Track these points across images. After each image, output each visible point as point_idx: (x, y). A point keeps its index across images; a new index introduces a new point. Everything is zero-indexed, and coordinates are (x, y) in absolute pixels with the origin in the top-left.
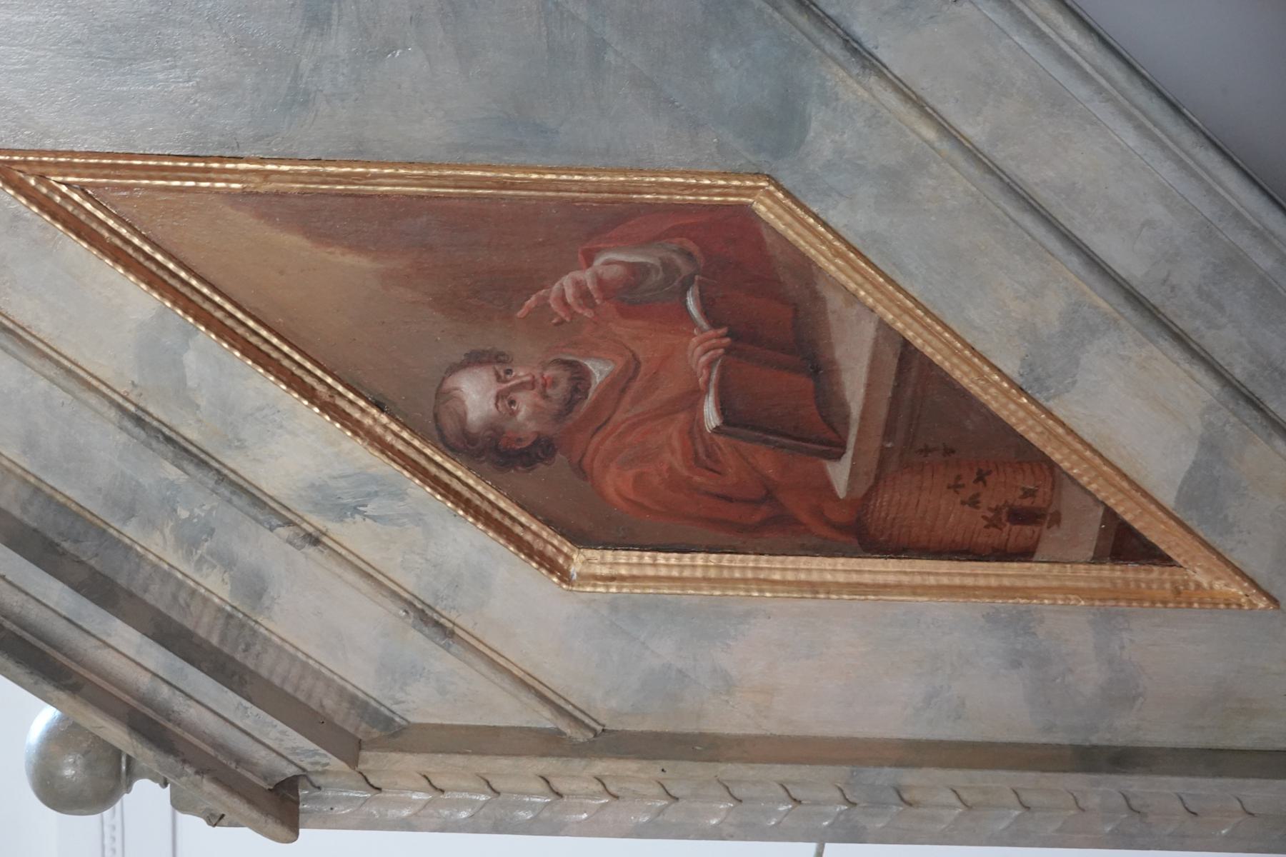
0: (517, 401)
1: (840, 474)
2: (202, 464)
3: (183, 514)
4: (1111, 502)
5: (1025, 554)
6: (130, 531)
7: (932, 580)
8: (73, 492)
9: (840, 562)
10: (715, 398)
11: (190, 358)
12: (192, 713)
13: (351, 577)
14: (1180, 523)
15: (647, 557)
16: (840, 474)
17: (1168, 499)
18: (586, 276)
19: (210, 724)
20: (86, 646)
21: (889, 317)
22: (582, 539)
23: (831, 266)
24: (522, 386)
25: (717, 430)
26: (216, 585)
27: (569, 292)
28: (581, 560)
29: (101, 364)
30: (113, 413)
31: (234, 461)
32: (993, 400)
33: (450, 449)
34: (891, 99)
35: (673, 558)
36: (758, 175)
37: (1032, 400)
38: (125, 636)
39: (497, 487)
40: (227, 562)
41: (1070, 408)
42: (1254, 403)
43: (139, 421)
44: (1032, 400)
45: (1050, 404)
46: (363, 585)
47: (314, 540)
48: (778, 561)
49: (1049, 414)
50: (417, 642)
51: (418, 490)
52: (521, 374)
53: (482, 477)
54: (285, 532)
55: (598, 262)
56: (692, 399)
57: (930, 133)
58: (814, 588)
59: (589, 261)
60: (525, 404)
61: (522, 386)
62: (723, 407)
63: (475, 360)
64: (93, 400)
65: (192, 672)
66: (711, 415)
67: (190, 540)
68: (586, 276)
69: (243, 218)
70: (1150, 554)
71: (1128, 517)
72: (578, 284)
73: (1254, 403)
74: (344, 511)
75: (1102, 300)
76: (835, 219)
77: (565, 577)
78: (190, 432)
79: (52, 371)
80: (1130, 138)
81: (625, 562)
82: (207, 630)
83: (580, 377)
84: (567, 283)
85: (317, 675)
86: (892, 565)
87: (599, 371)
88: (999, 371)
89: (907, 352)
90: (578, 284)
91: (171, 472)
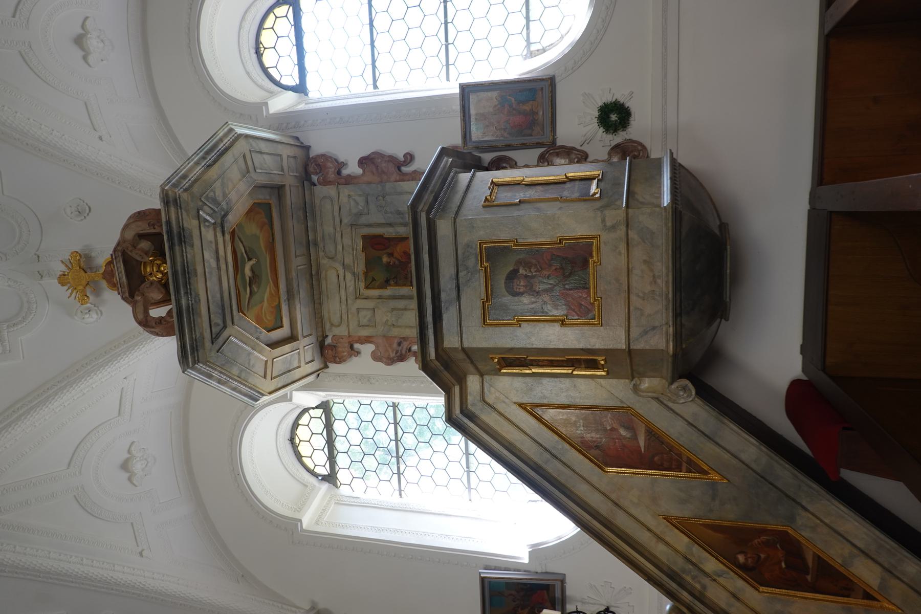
0: (362, 353)
1: (809, 578)
2: (696, 566)
3: (693, 574)
4: (864, 588)
5: (848, 596)
6: (684, 576)
7: (830, 599)
8: (675, 568)
9: (811, 594)
10: (806, 453)
11: (694, 549)
12: (696, 608)
13: (721, 587)
14: (880, 594)
15: (774, 589)
16: (809, 578)
17: (876, 589)
18: (759, 540)
19: (699, 610)
20: (680, 595)
21: (815, 551)
22: (762, 585)
23: (804, 542)
24: (749, 558)
25: (785, 568)
26: (698, 586)
27: (757, 543)
28: (761, 589)
29: (679, 548)
30: (681, 556)
31: (701, 566)
32: (837, 567)
33: (736, 567)
34: (811, 516)
35: (778, 590)
36: (788, 526)
37: (845, 568)
38: (685, 594)
39: (746, 574)
40: (699, 582)
41: (852, 570)
42: (890, 572)
43: (686, 558)
44: (845, 568)
45: (849, 569)
46: (723, 589)
47: (715, 580)
48: (798, 593)
49: (849, 571)
50: (733, 600)
51: (732, 573)
52: (749, 555)
53: (743, 572)
54: (710, 579)
55: (761, 538)
56: (780, 562)
57: (819, 522)
58: (806, 598)
59: (759, 537)
60: (750, 560)
61: (749, 558)
62: (786, 564)
63: (741, 552)
64: (678, 554)
65: (696, 601)
66: (783, 565)
67: (694, 578)
68: (759, 540)
69: (516, 407)
70: (874, 599)
71: (868, 591)
72: (758, 542)
73: (890, 572)
74: (719, 576)
75: (855, 551)
76: (803, 534)
77: (759, 591)
78: (694, 560)
79: (672, 549)
80: (857, 524)
81: (770, 590)
82: (697, 594)
83: (759, 557)
84: (756, 541)
85: (715, 604)
86: (821, 595)
87: (763, 556)
88: (838, 562)
89: (819, 557)
90: (758, 542)
91: (691, 567)
